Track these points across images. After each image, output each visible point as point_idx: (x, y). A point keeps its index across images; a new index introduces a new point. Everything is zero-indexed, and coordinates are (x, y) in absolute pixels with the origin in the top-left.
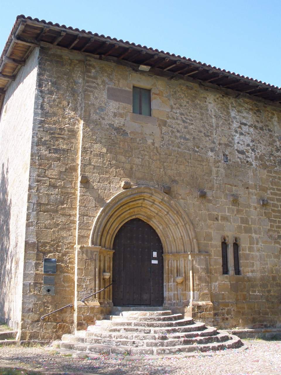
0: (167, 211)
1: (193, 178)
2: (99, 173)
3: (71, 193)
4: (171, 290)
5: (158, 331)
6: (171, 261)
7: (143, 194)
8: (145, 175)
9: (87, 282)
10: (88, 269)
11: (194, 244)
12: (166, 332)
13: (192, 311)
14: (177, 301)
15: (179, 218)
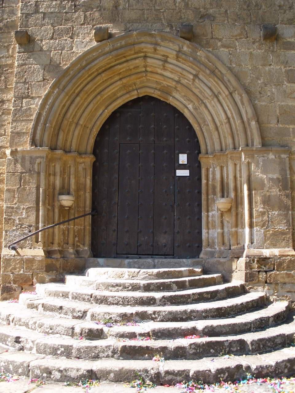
0: (194, 72)
1: (248, 6)
2: (52, 24)
3: (7, 65)
4: (214, 227)
5: (99, 315)
6: (214, 168)
7: (137, 47)
8: (143, 14)
9: (22, 213)
10: (24, 189)
11: (251, 131)
12: (118, 319)
13: (246, 268)
14: (222, 248)
15: (217, 83)
